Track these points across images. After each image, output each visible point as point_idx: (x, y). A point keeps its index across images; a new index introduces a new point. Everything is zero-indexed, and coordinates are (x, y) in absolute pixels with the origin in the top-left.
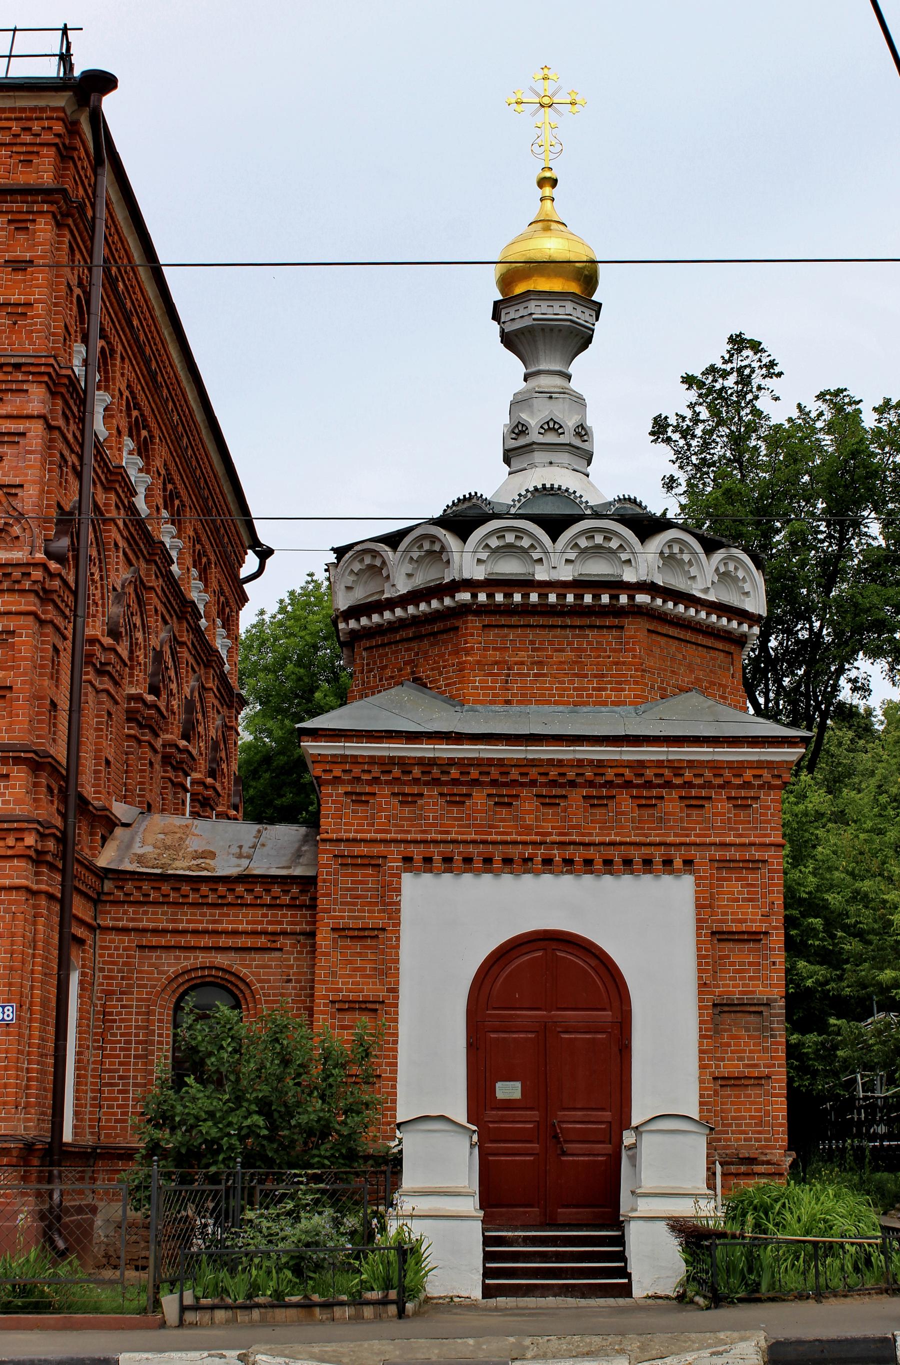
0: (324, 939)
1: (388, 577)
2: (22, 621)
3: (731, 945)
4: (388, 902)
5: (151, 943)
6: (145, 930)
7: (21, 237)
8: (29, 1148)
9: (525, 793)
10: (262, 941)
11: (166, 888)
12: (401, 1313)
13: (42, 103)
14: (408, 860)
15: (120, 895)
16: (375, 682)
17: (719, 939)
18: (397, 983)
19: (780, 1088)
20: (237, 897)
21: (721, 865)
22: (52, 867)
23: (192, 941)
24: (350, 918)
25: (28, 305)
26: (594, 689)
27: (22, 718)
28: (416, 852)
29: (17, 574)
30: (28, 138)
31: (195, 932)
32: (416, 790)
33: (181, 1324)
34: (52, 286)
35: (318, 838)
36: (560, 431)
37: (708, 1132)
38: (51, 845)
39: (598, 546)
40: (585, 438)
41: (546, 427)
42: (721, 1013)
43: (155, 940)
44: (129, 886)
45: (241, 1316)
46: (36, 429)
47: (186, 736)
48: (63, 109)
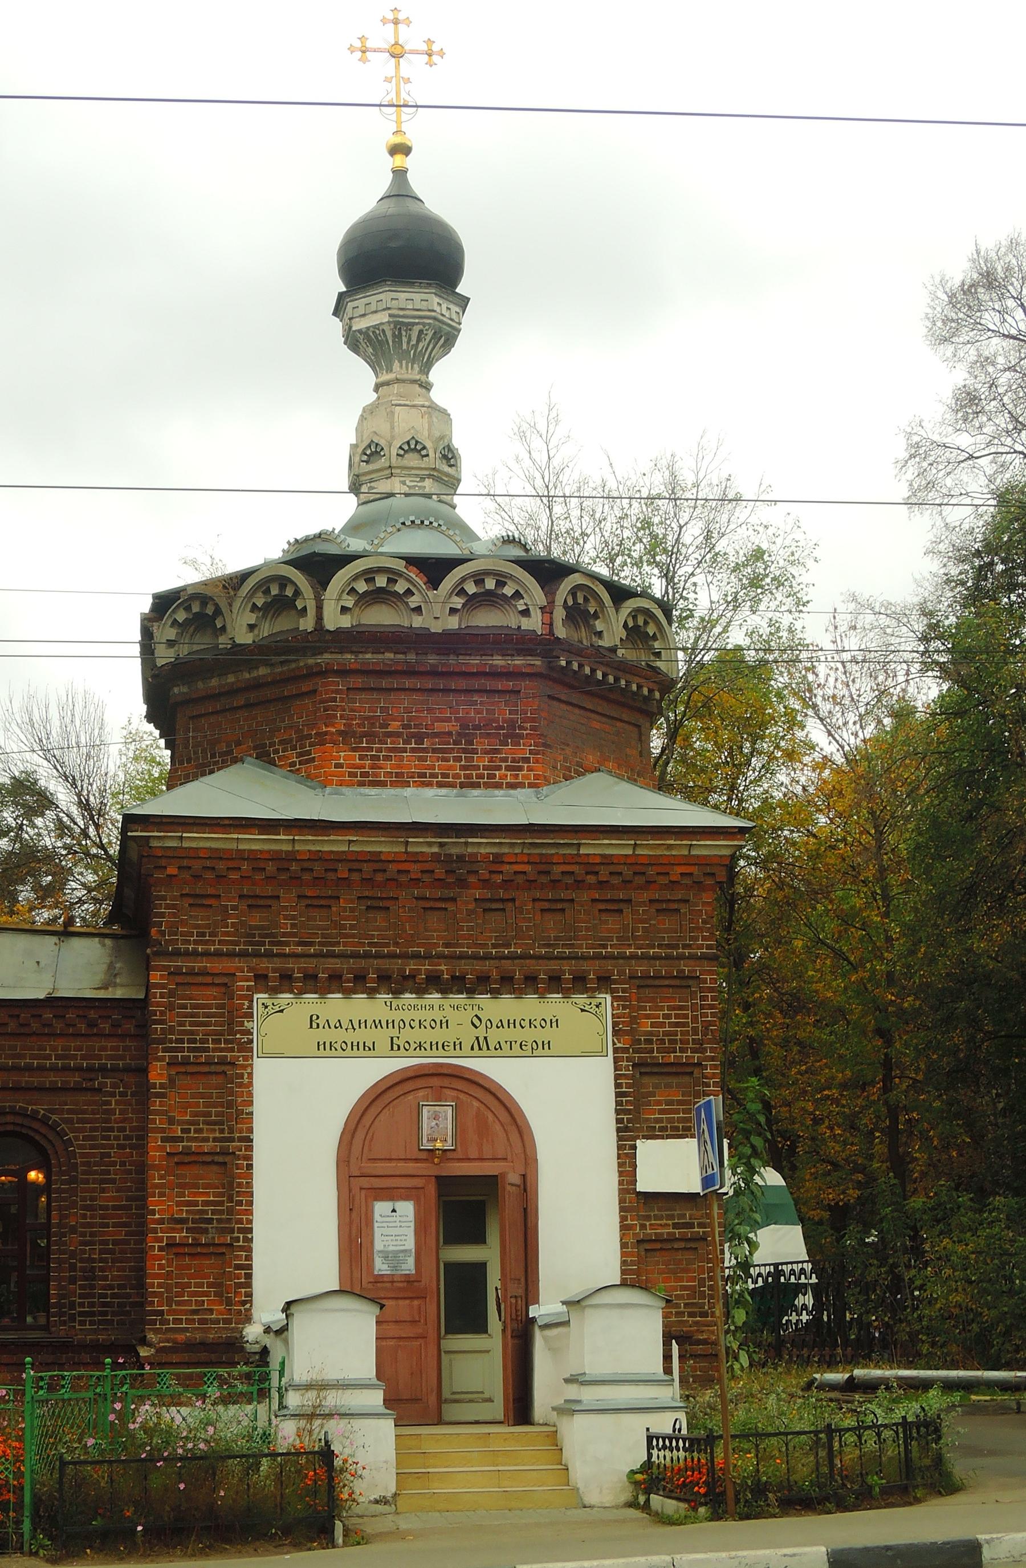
1: (223, 629)
3: (655, 1080)
9: (403, 894)
16: (205, 757)
18: (251, 1130)
19: (152, 1285)
20: (44, 1025)
21: (642, 982)
24: (190, 1050)
26: (485, 768)
32: (269, 890)
35: (149, 951)
36: (424, 452)
37: (663, 1304)
39: (489, 593)
40: (452, 462)
41: (406, 447)
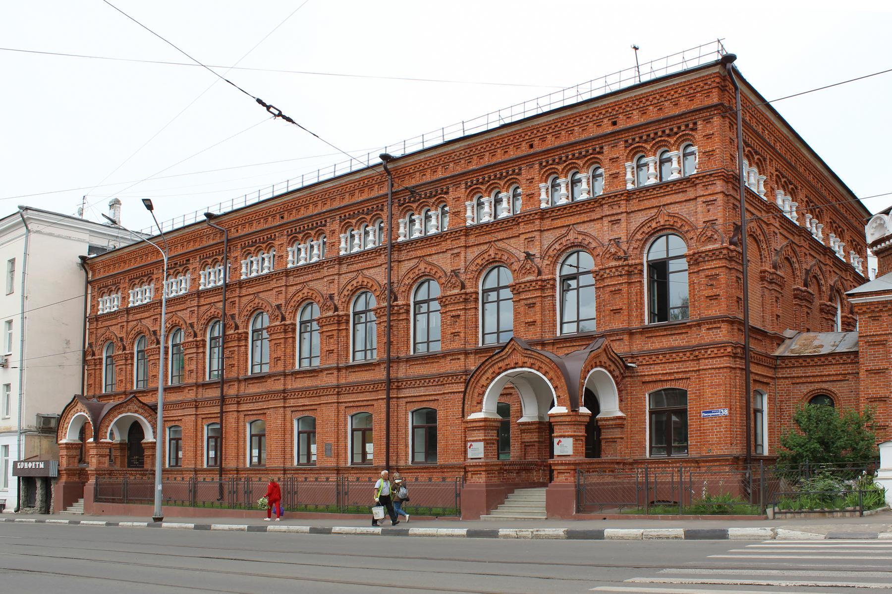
0: (862, 374)
2: (721, 270)
5: (796, 381)
6: (794, 377)
7: (708, 125)
8: (736, 459)
10: (840, 377)
11: (801, 361)
12: (862, 515)
13: (675, 83)
15: (784, 365)
22: (741, 358)
23: (812, 380)
25: (713, 150)
27: (724, 305)
29: (717, 253)
30: (707, 87)
31: (813, 376)
33: (774, 518)
34: (722, 141)
38: (739, 350)
43: (798, 381)
44: (787, 361)
45: (797, 516)
46: (720, 197)
47: (831, 300)
48: (718, 72)
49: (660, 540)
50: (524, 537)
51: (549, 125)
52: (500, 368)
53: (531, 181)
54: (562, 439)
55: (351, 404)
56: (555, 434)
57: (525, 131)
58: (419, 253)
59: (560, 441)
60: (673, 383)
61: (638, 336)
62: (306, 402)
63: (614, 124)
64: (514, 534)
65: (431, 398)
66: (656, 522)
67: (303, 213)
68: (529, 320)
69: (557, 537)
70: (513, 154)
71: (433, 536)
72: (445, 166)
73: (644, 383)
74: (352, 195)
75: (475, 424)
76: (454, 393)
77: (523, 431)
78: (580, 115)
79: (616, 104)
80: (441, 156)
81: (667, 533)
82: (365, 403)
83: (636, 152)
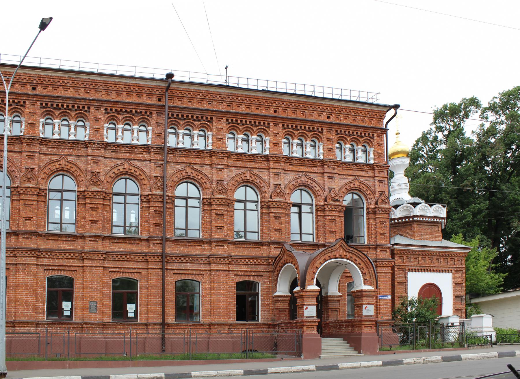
4: (405, 277)
13: (365, 108)
14: (409, 269)
17: (456, 284)
28: (410, 268)
42: (456, 297)
49: (488, 359)
50: (419, 363)
51: (291, 102)
52: (356, 260)
53: (276, 135)
54: (367, 306)
55: (117, 270)
56: (298, 304)
57: (275, 100)
58: (189, 160)
59: (366, 307)
60: (130, 274)
61: (107, 241)
62: (64, 262)
63: (328, 117)
64: (413, 361)
65: (197, 272)
66: (484, 350)
67: (60, 92)
68: (277, 228)
69: (437, 361)
70: (262, 111)
71: (358, 367)
72: (210, 101)
73: (347, 277)
74: (119, 94)
75: (311, 293)
76: (220, 270)
77: (276, 301)
78: (311, 104)
79: (333, 106)
80: (208, 93)
81: (491, 355)
82: (132, 270)
83: (113, 120)
